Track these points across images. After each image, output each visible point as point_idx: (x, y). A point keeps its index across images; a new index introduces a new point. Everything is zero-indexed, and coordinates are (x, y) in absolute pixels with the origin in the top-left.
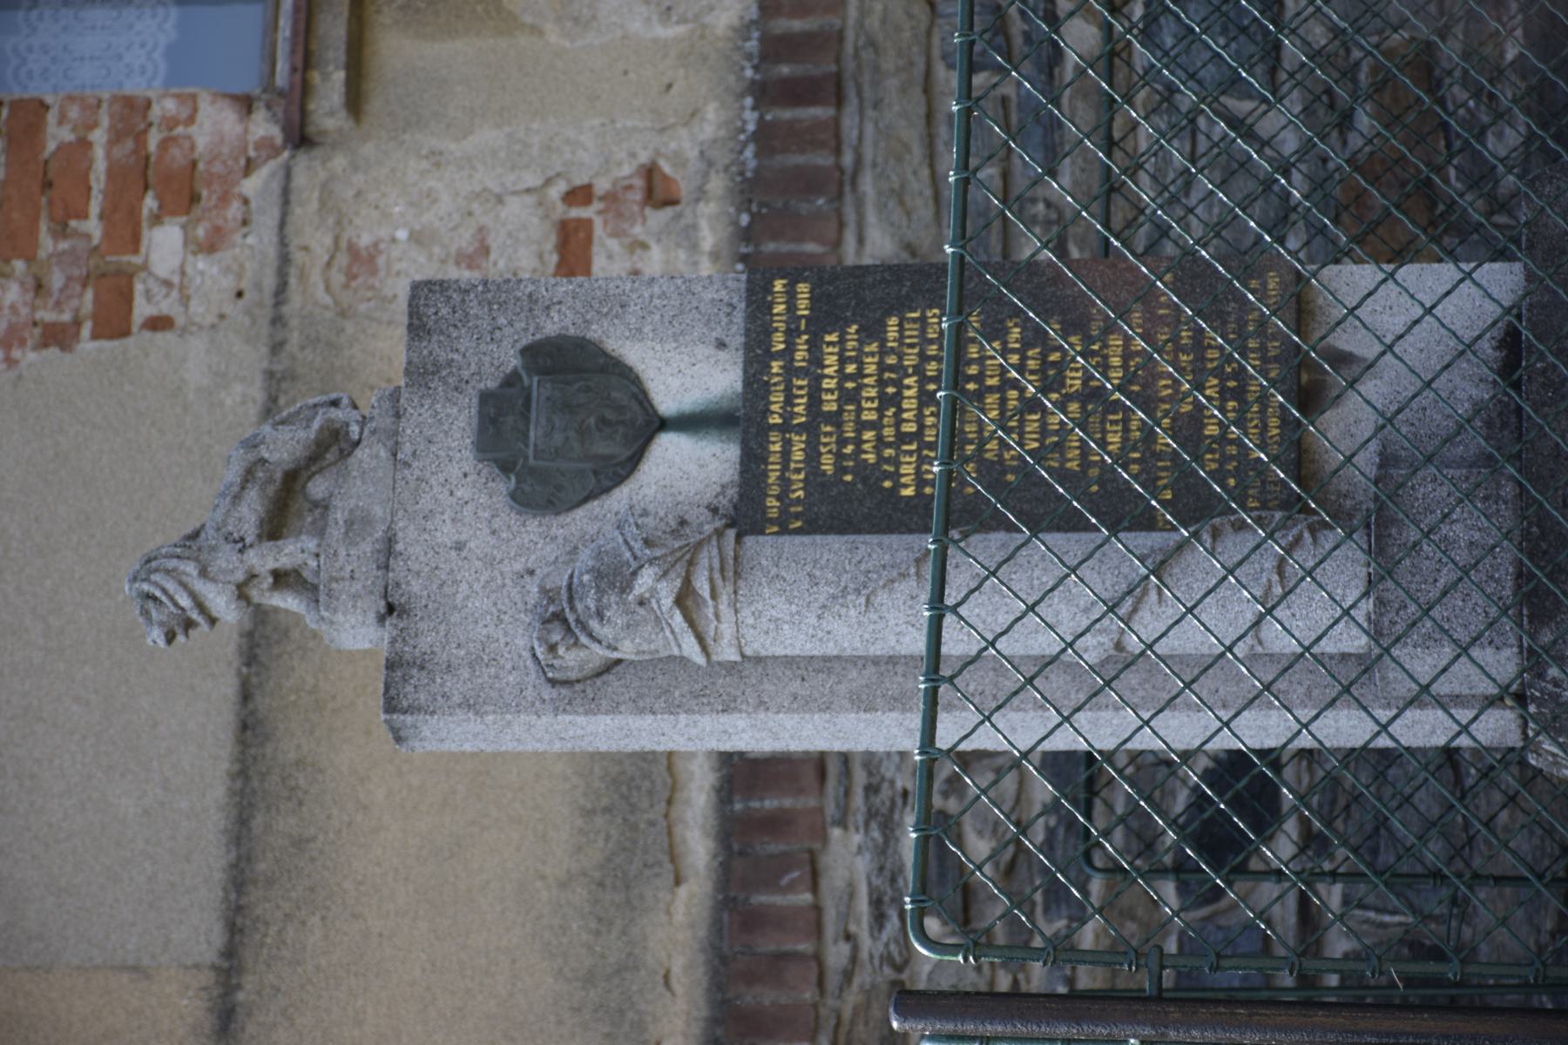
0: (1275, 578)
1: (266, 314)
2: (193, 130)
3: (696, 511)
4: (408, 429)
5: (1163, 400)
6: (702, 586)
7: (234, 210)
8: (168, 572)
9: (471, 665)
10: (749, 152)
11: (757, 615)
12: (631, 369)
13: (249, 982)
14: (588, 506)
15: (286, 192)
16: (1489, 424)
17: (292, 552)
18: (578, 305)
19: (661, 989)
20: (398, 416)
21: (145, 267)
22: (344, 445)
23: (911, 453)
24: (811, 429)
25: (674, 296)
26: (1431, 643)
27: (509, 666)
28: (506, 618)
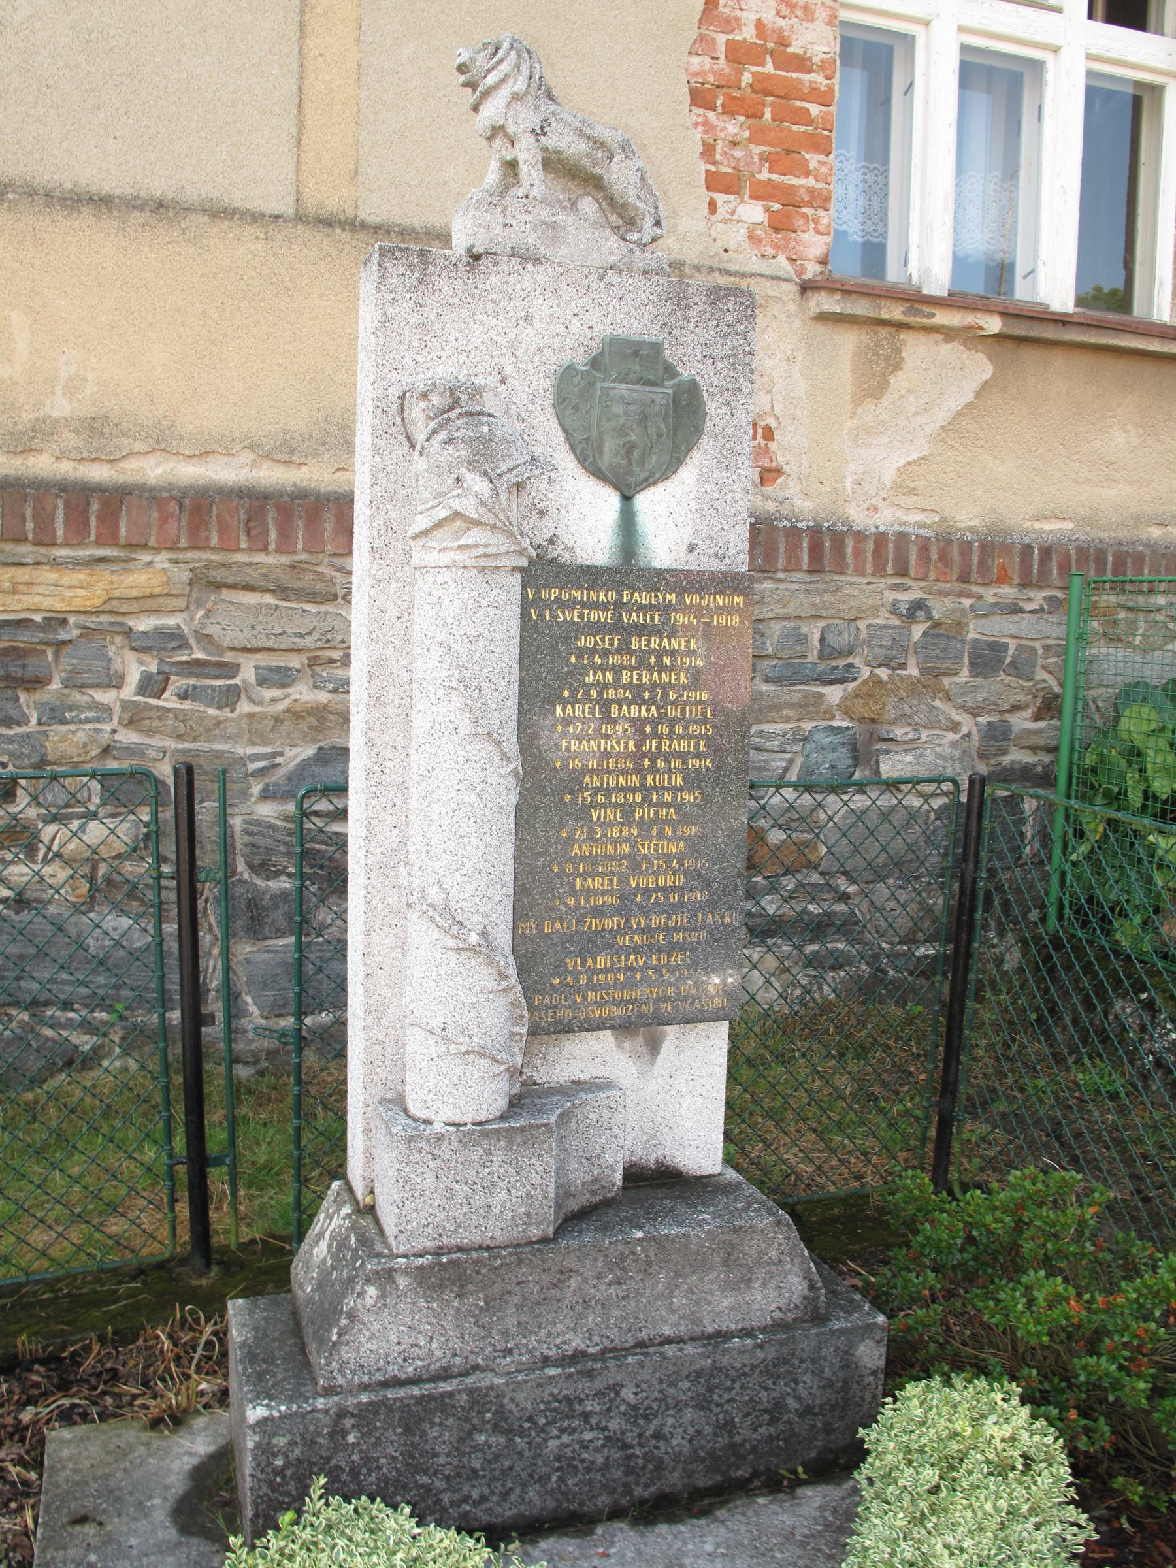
0: (464, 1049)
1: (716, 265)
2: (812, 232)
3: (551, 526)
4: (635, 281)
5: (627, 920)
6: (474, 536)
7: (770, 251)
8: (517, 66)
9: (421, 325)
10: (786, 523)
11: (444, 586)
12: (675, 472)
13: (346, 236)
14: (560, 433)
15: (778, 278)
16: (595, 1180)
17: (531, 174)
18: (729, 430)
19: (337, 466)
20: (645, 273)
21: (743, 201)
22: (623, 229)
23: (592, 713)
24: (617, 627)
25: (733, 511)
26: (401, 1183)
27: (419, 358)
28: (463, 357)
